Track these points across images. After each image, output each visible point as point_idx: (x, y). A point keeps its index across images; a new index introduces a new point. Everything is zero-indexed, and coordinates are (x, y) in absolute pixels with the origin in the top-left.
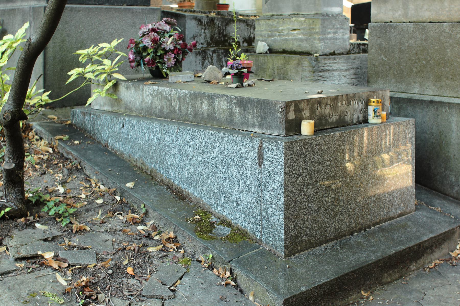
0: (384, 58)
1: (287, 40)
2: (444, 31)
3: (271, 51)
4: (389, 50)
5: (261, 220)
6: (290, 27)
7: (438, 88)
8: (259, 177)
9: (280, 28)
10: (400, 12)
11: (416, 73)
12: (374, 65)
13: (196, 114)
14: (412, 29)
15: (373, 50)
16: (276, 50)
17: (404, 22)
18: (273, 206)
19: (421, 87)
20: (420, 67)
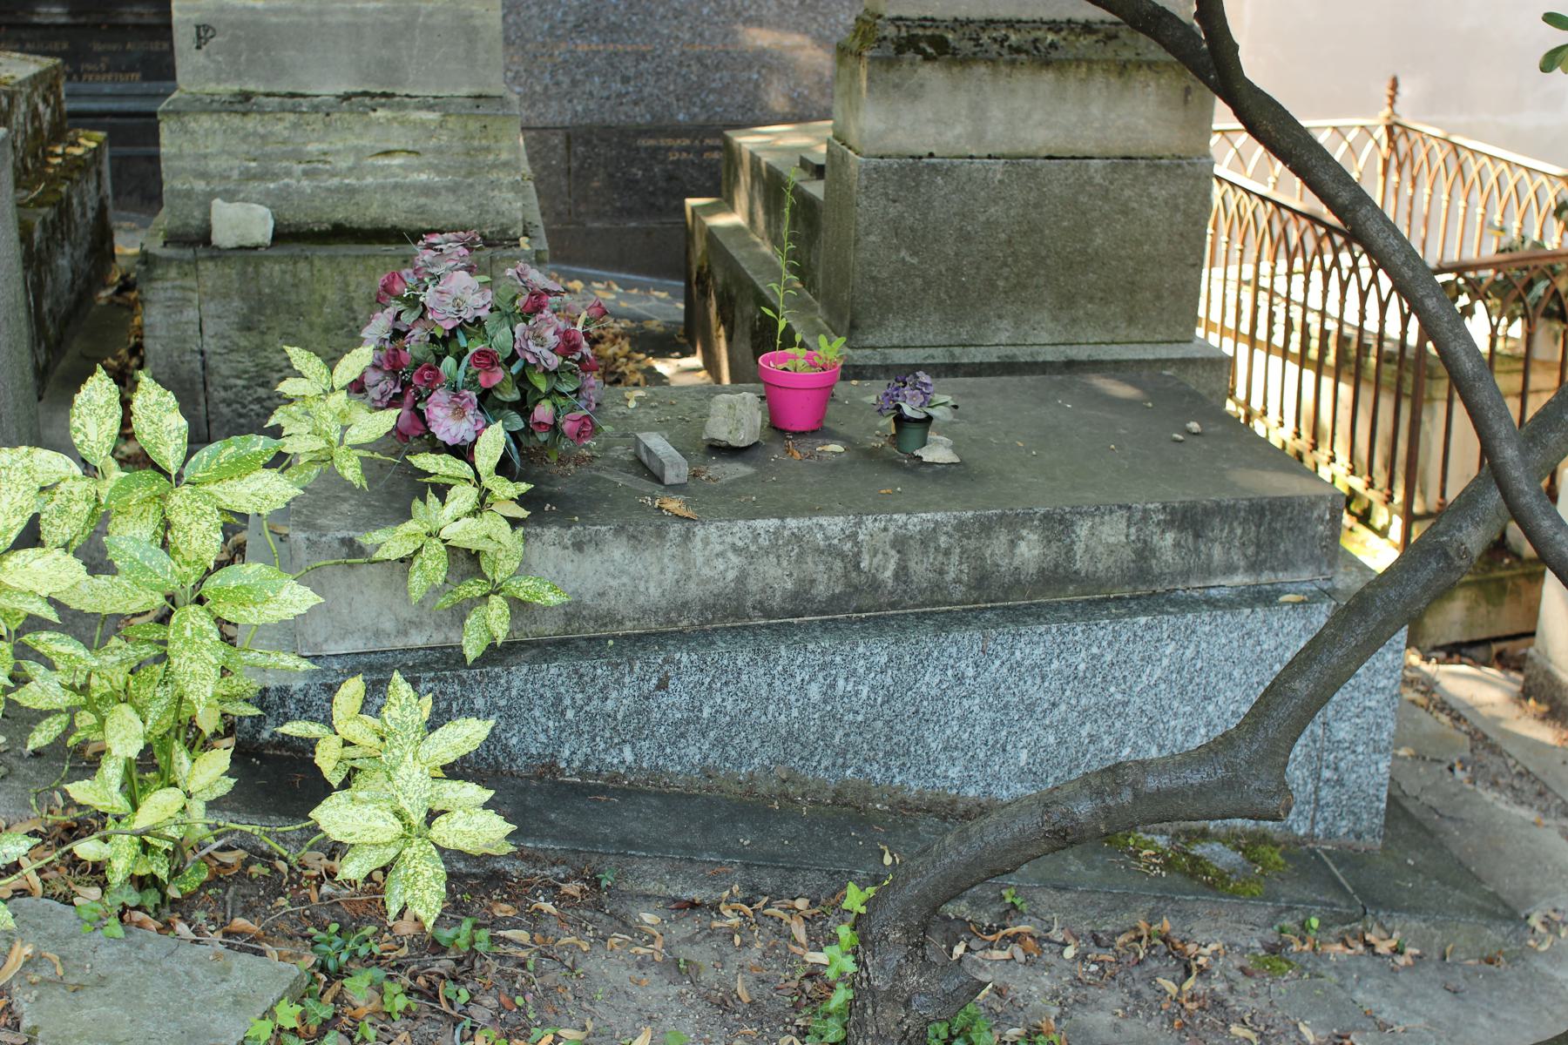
1: (352, 191)
3: (284, 235)
4: (924, 236)
5: (1317, 789)
6: (365, 142)
7: (1065, 326)
9: (313, 147)
10: (959, 129)
12: (873, 279)
13: (982, 580)
14: (999, 176)
15: (872, 238)
16: (298, 225)
17: (971, 157)
18: (1360, 749)
19: (1017, 326)
20: (1018, 275)
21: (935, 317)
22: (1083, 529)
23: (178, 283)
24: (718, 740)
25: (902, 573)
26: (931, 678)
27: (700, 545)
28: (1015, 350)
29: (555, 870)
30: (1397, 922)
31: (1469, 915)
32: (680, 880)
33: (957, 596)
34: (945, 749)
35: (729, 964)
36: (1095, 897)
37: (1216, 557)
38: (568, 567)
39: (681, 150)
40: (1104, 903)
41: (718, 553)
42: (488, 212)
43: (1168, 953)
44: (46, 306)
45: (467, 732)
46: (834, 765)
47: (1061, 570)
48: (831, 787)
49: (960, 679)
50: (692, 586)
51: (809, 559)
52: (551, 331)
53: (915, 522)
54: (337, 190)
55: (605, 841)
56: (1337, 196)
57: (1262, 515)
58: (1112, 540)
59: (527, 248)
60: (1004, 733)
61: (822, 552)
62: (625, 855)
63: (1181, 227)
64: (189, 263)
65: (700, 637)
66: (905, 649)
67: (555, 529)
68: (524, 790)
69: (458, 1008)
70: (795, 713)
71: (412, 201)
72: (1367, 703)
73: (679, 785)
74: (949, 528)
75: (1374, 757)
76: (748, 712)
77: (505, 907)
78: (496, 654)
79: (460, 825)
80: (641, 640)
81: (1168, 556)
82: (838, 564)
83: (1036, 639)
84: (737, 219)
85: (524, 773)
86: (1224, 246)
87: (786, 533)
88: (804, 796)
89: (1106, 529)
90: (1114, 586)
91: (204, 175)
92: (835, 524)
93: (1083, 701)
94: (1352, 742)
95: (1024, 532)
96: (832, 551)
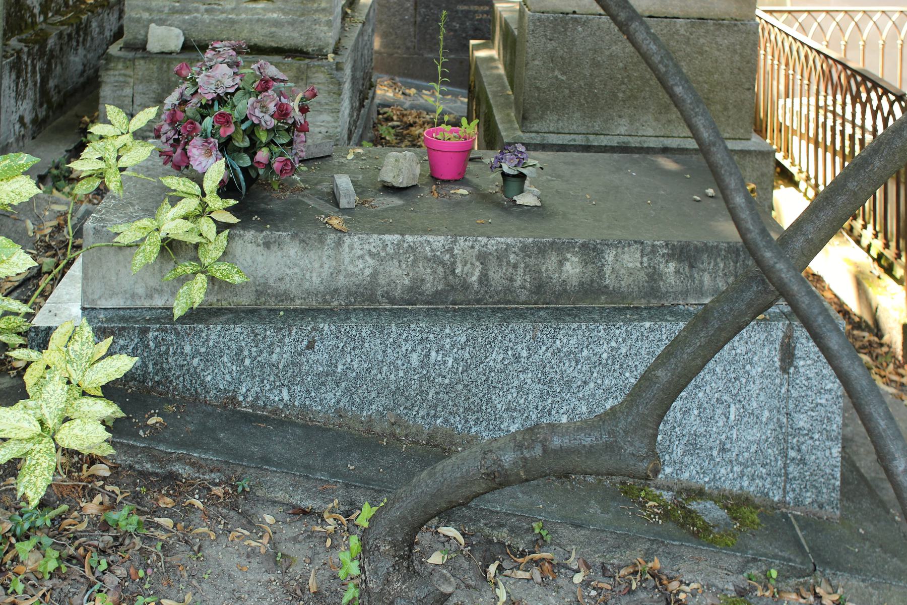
0: (559, 76)
1: (233, 22)
2: (677, 32)
5: (785, 466)
7: (663, 125)
8: (783, 390)
11: (624, 101)
12: (538, 89)
13: (539, 287)
15: (536, 62)
18: (816, 436)
19: (631, 122)
20: (631, 90)
21: (577, 115)
22: (610, 256)
23: (122, 72)
24: (348, 389)
25: (484, 279)
26: (496, 356)
27: (347, 250)
28: (630, 139)
29: (213, 475)
30: (841, 580)
31: (900, 580)
32: (299, 492)
33: (523, 298)
34: (507, 409)
35: (316, 561)
36: (603, 535)
37: (706, 283)
38: (260, 259)
39: (483, 13)
40: (611, 541)
41: (357, 257)
42: (311, 38)
43: (656, 587)
44: (52, 83)
45: (119, 364)
46: (428, 415)
47: (595, 284)
48: (426, 432)
49: (517, 358)
50: (341, 277)
51: (421, 265)
52: (273, 104)
53: (493, 244)
54: (224, 21)
55: (251, 458)
56: (617, 15)
57: (738, 255)
58: (630, 265)
59: (332, 60)
60: (550, 401)
61: (429, 260)
62: (261, 469)
63: (739, 64)
64: (130, 60)
65: (344, 314)
66: (478, 333)
67: (252, 232)
68: (209, 415)
69: (97, 574)
70: (401, 374)
71: (267, 30)
72: (819, 401)
73: (320, 420)
74: (516, 249)
75: (828, 443)
76: (368, 371)
77: (168, 500)
78: (196, 315)
79: (77, 431)
80: (302, 313)
81: (672, 280)
82: (440, 270)
83: (570, 332)
84: (493, 53)
85: (214, 402)
86: (799, 82)
87: (405, 245)
88: (406, 436)
89: (626, 257)
90: (633, 299)
91: (149, 10)
92: (438, 241)
93: (607, 382)
94: (809, 430)
95: (569, 256)
96: (435, 260)
